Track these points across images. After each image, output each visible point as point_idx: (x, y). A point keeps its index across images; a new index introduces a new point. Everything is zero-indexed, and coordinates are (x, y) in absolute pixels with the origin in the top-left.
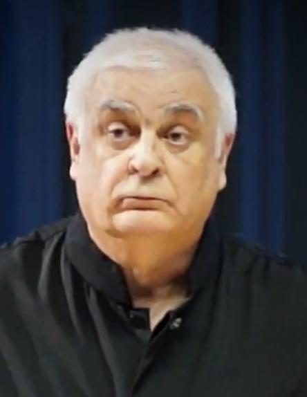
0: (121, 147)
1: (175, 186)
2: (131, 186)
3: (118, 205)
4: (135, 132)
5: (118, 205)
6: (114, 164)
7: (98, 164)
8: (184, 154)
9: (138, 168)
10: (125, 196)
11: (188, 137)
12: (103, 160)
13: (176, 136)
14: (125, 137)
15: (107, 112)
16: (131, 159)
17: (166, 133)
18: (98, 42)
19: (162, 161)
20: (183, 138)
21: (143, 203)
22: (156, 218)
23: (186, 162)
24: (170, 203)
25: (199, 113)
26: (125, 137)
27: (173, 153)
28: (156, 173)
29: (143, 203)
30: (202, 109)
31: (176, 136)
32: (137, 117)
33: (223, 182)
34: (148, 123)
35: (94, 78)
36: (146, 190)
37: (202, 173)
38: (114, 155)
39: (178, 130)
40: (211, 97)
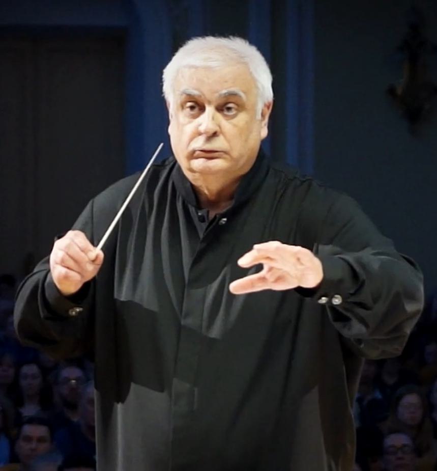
0: (195, 117)
1: (228, 141)
2: (199, 143)
3: (192, 156)
4: (202, 109)
5: (192, 156)
6: (190, 128)
7: (181, 126)
8: (235, 121)
9: (202, 132)
10: (197, 149)
11: (236, 110)
12: (184, 125)
13: (229, 109)
14: (196, 110)
15: (184, 96)
16: (200, 125)
17: (222, 108)
18: (181, 46)
19: (220, 127)
20: (233, 110)
21: (209, 154)
22: (218, 164)
23: (235, 126)
24: (225, 152)
25: (242, 94)
26: (196, 110)
27: (227, 120)
28: (215, 134)
29: (209, 154)
30: (245, 93)
31: (229, 109)
32: (201, 100)
33: (264, 133)
34: (210, 103)
35: (178, 71)
36: (208, 147)
37: (245, 131)
38: (190, 122)
39: (230, 105)
40: (252, 82)
